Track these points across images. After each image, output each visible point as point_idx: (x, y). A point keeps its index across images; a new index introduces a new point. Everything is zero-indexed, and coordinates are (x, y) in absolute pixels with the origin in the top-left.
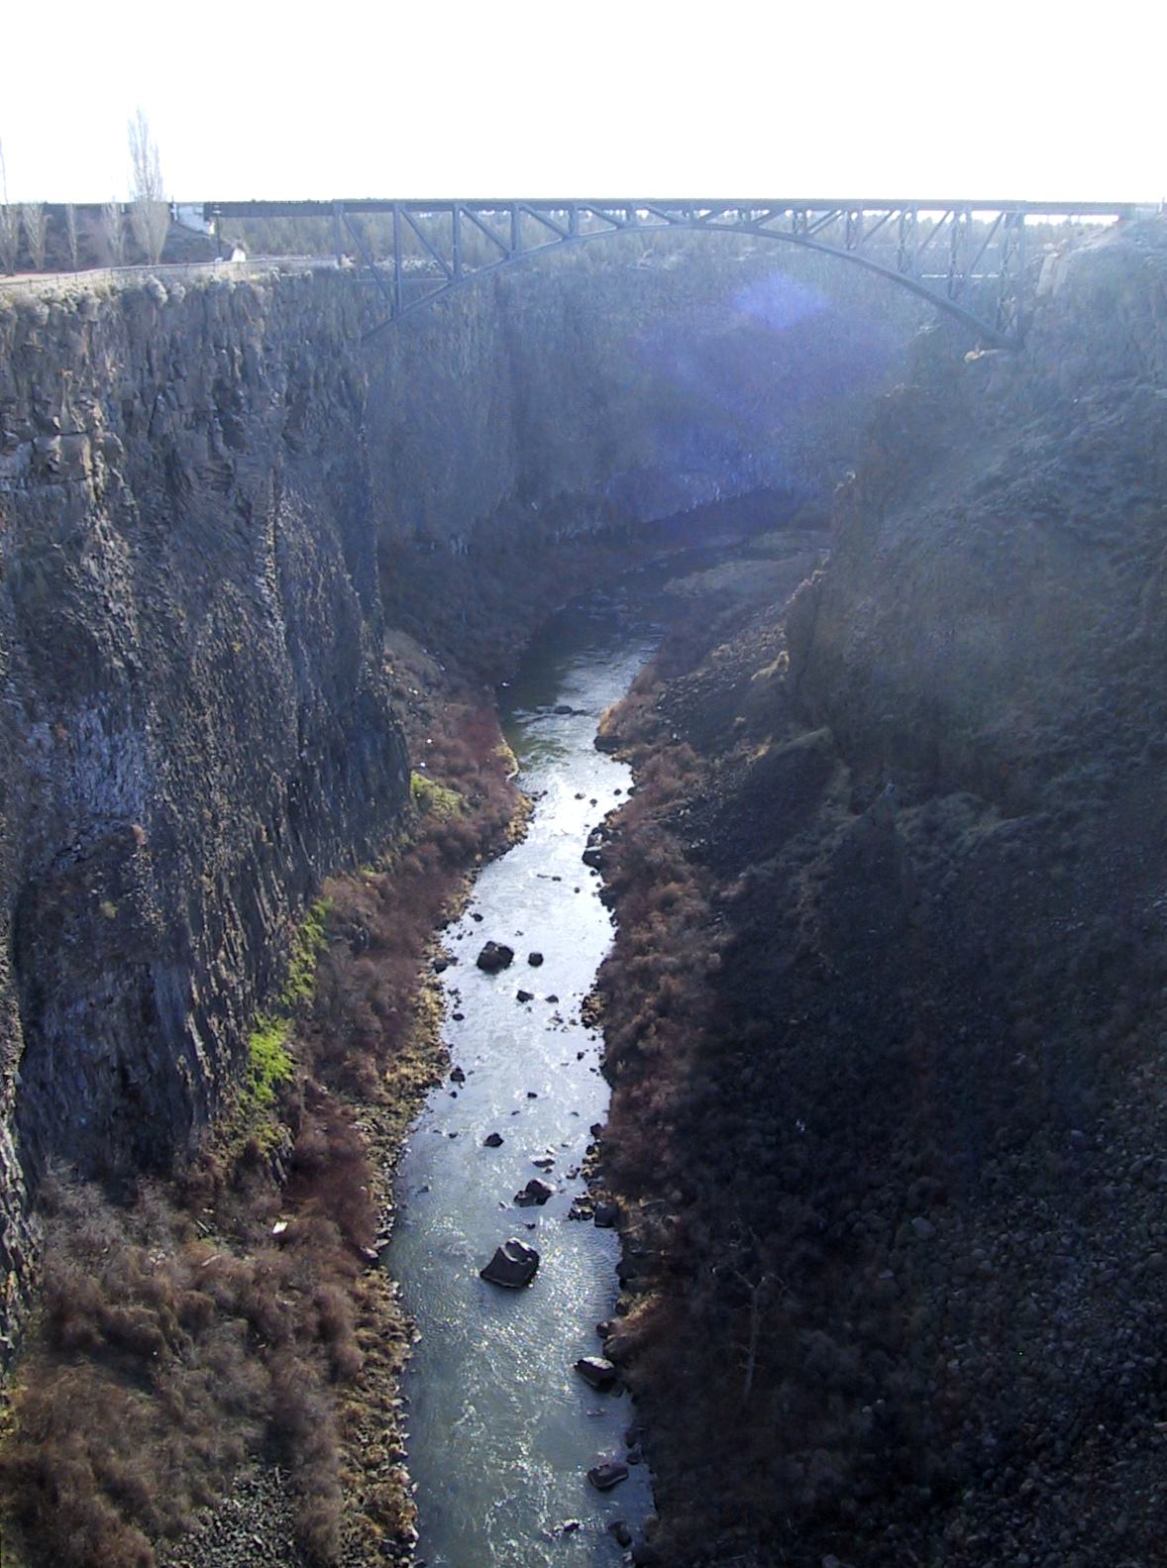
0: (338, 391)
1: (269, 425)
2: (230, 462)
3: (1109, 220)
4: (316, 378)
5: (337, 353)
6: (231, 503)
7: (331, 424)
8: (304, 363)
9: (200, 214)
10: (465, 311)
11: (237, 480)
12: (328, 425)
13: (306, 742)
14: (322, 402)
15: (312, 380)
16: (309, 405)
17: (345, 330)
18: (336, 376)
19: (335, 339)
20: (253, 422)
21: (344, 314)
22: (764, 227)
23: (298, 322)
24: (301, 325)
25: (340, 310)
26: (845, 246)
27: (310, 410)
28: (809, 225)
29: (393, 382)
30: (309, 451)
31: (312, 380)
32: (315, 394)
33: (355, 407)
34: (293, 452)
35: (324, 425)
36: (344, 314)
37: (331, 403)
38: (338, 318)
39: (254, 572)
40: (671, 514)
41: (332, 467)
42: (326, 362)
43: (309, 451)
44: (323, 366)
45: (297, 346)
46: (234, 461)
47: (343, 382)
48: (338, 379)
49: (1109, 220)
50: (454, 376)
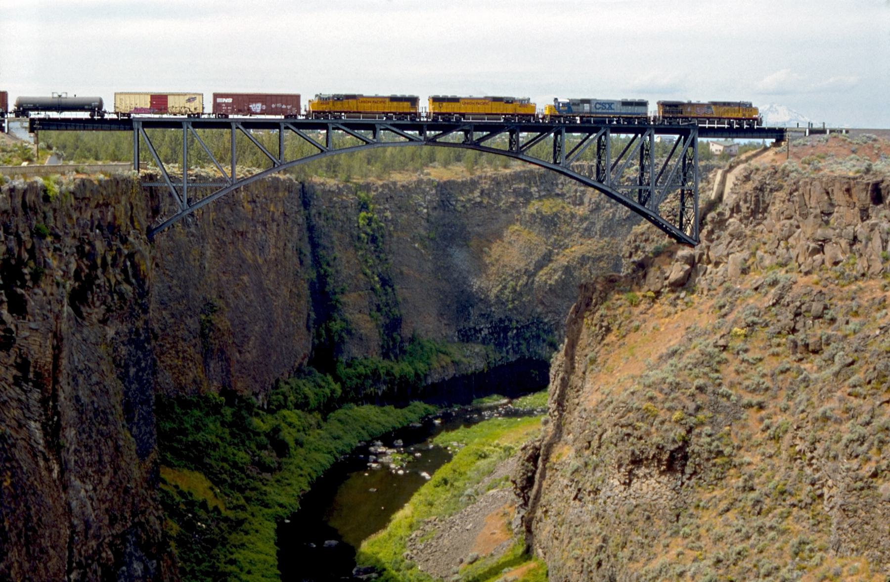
0: (124, 271)
1: (51, 297)
2: (13, 327)
3: (230, 100)
4: (104, 259)
5: (124, 241)
6: (11, 361)
7: (116, 297)
8: (93, 247)
9: (26, 128)
10: (272, 209)
11: (17, 342)
12: (113, 299)
13: (74, 565)
14: (109, 280)
15: (99, 261)
16: (97, 282)
17: (132, 222)
18: (122, 259)
19: (123, 228)
20: (35, 294)
21: (132, 208)
22: (482, 144)
23: (89, 215)
24: (92, 216)
25: (129, 206)
26: (552, 161)
27: (99, 286)
28: (521, 145)
29: (207, 265)
30: (95, 320)
31: (99, 261)
32: (103, 273)
33: (139, 284)
34: (79, 320)
35: (110, 298)
36: (132, 208)
37: (117, 280)
38: (126, 213)
39: (29, 418)
40: (446, 378)
41: (117, 333)
42: (114, 248)
43: (95, 320)
44: (111, 250)
45: (86, 234)
46: (16, 326)
47: (128, 263)
48: (125, 262)
49: (230, 100)
50: (260, 261)
